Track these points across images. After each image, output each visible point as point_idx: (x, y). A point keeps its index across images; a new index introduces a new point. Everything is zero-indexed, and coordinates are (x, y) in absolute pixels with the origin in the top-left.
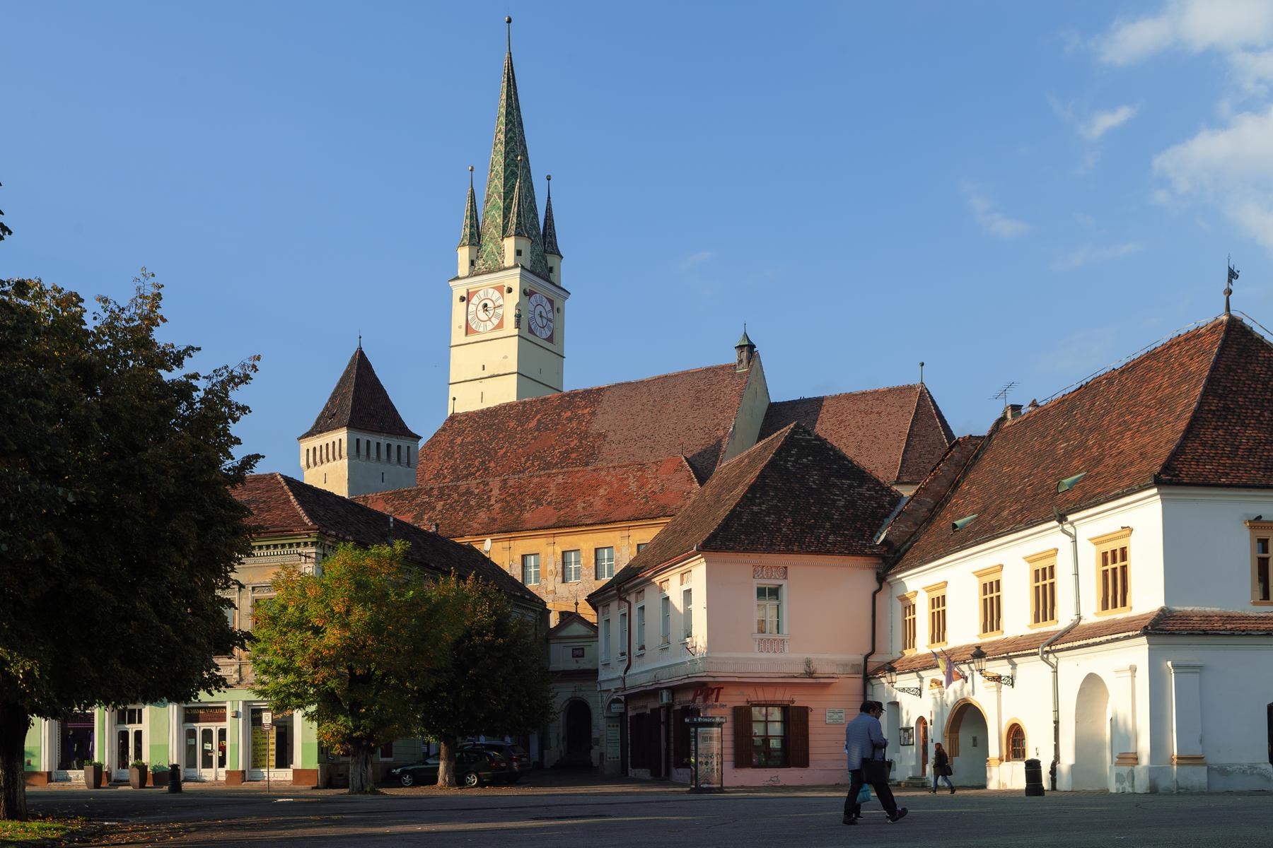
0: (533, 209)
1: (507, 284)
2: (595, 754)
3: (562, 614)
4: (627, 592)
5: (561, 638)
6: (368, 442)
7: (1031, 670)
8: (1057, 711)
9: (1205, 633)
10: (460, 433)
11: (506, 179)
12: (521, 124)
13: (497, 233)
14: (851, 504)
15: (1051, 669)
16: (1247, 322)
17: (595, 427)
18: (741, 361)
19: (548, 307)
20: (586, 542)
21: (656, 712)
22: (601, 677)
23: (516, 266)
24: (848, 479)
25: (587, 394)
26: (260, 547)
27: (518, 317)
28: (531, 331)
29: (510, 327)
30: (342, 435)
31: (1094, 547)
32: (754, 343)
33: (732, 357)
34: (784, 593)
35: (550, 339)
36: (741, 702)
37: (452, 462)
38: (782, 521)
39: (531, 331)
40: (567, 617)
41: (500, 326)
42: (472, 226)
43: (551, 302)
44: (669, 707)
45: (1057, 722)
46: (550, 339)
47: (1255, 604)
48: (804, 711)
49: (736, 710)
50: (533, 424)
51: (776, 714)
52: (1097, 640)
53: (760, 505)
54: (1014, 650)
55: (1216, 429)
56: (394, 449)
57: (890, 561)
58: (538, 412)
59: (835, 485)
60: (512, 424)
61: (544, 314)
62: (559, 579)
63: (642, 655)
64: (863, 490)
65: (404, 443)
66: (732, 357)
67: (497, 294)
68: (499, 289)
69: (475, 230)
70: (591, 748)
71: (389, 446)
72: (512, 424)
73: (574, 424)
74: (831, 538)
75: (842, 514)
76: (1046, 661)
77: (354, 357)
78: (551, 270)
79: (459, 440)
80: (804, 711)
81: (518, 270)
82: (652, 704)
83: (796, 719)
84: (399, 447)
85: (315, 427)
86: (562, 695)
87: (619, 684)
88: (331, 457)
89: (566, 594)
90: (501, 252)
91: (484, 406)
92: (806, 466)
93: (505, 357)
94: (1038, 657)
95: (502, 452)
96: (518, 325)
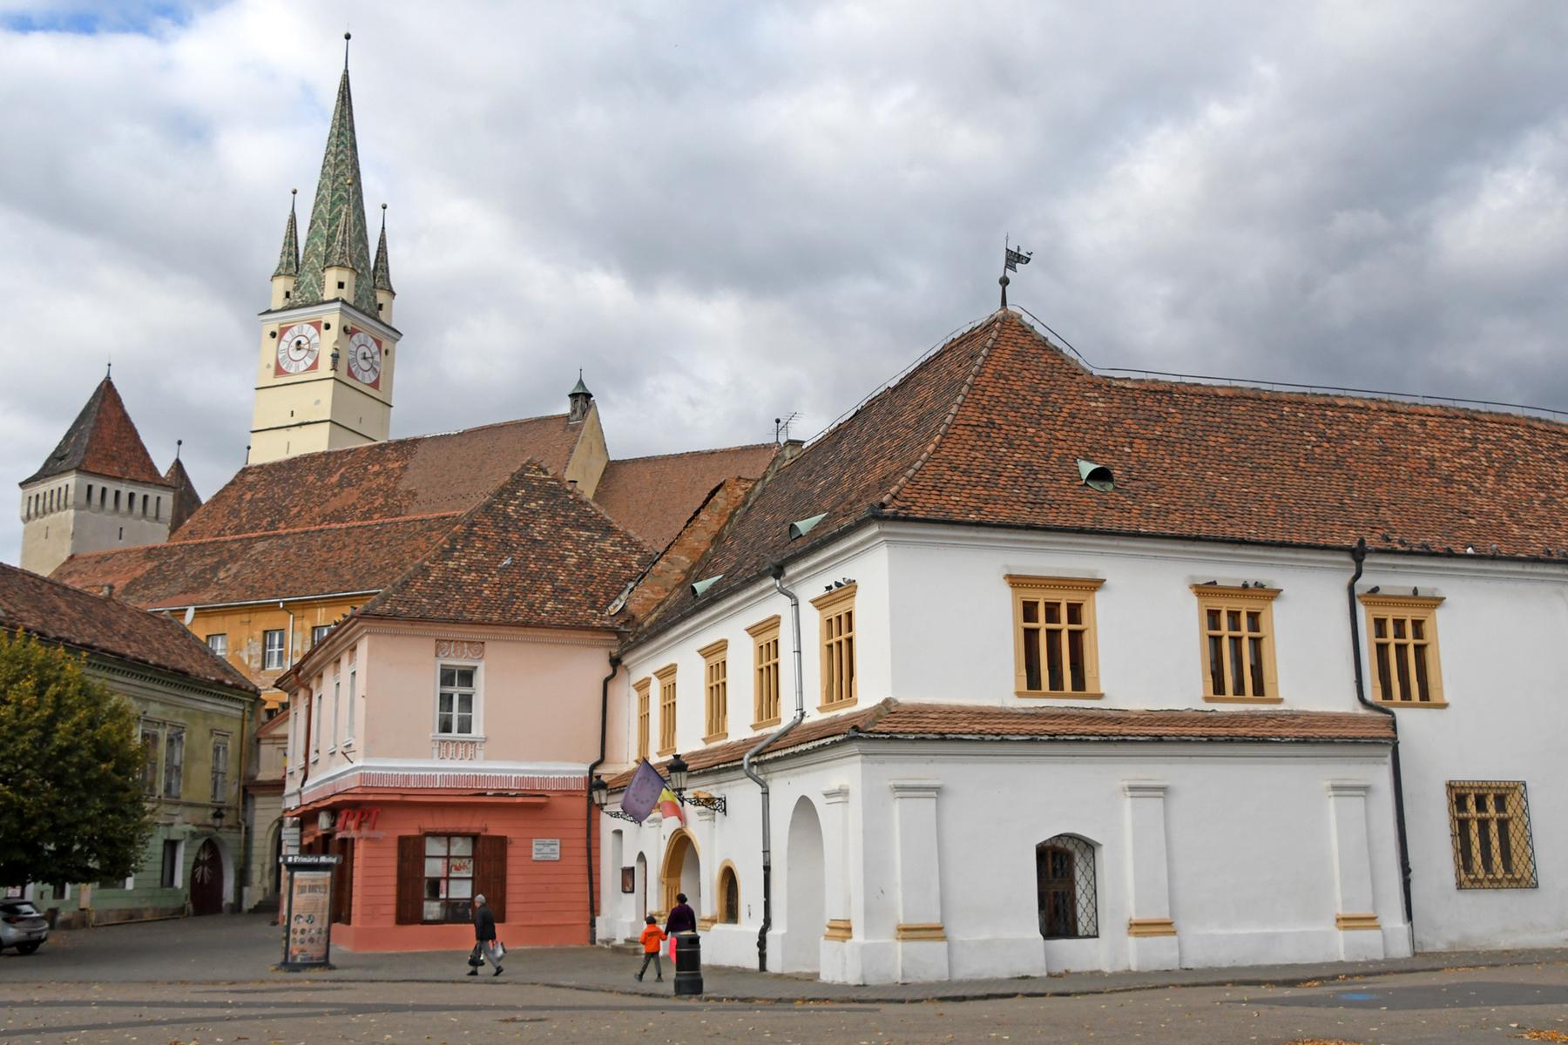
0: (362, 238)
1: (325, 320)
5: (275, 738)
7: (741, 794)
8: (766, 852)
9: (942, 738)
10: (251, 487)
11: (333, 204)
12: (354, 147)
14: (587, 562)
15: (759, 789)
16: (1027, 319)
17: (403, 486)
18: (574, 412)
19: (374, 348)
23: (336, 300)
24: (588, 529)
25: (402, 443)
27: (335, 357)
28: (350, 374)
29: (325, 368)
30: (71, 480)
31: (817, 613)
32: (590, 390)
33: (565, 408)
34: (479, 679)
35: (375, 385)
36: (412, 831)
37: (236, 521)
38: (485, 580)
39: (350, 374)
41: (314, 366)
42: (290, 254)
43: (379, 343)
45: (767, 869)
46: (375, 385)
47: (1019, 694)
48: (502, 842)
49: (402, 841)
50: (335, 479)
51: (461, 847)
52: (803, 747)
54: (725, 763)
55: (973, 448)
56: (138, 500)
57: (628, 638)
58: (341, 466)
59: (568, 537)
60: (311, 478)
64: (607, 545)
66: (565, 408)
67: (313, 330)
68: (316, 325)
69: (292, 259)
71: (131, 496)
72: (311, 478)
73: (381, 480)
74: (549, 605)
75: (571, 574)
76: (755, 779)
77: (99, 389)
78: (380, 307)
79: (248, 496)
80: (502, 842)
81: (338, 305)
83: (491, 859)
84: (117, 493)
85: (42, 469)
90: (321, 284)
91: (289, 456)
92: (532, 512)
93: (318, 402)
94: (741, 774)
95: (295, 510)
96: (334, 368)
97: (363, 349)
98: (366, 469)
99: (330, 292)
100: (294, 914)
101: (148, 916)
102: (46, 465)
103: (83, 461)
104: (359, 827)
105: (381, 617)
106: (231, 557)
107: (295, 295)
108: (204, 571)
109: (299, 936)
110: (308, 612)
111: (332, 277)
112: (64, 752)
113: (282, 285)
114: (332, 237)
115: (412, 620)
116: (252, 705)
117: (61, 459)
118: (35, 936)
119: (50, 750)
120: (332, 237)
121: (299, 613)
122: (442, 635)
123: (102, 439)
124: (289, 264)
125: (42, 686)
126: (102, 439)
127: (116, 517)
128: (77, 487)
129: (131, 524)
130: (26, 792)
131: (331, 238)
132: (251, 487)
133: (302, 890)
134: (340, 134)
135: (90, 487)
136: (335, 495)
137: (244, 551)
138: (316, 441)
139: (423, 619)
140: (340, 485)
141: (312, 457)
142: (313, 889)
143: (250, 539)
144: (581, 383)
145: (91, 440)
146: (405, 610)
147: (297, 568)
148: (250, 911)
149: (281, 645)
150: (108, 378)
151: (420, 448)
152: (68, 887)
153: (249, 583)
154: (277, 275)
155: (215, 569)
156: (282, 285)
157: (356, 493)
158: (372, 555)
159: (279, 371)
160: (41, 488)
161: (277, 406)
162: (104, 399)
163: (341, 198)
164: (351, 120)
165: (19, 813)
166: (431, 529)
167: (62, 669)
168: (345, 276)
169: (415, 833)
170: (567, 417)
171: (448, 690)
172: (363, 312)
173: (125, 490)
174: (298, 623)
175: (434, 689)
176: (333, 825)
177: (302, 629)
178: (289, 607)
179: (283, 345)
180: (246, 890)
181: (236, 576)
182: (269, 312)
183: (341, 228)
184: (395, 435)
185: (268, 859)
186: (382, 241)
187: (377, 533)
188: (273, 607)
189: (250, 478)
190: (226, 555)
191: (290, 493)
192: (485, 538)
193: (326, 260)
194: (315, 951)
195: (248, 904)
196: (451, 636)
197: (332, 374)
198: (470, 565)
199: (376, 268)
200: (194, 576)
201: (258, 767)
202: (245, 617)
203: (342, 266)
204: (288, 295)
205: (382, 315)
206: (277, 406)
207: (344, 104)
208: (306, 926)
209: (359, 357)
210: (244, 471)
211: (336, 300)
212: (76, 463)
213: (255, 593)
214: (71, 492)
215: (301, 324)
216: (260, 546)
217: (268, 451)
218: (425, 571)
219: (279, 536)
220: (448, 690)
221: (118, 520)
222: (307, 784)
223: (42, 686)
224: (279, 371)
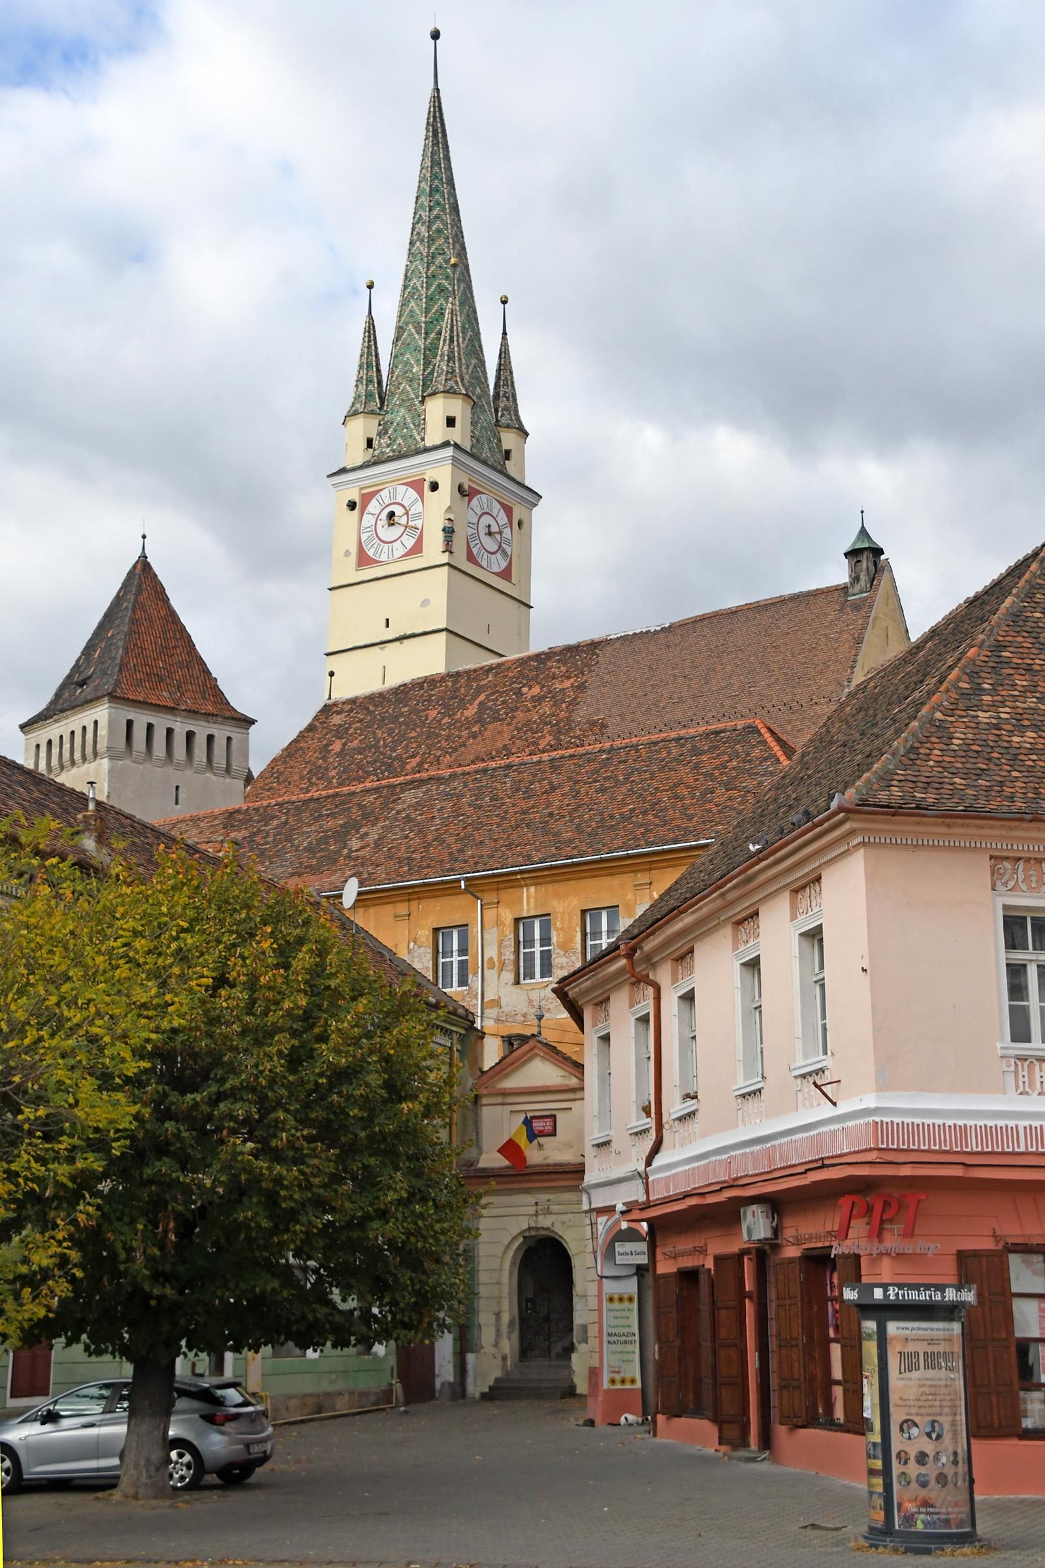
0: (475, 350)
1: (430, 475)
2: (579, 1363)
3: (510, 1041)
4: (651, 961)
5: (505, 1093)
6: (150, 727)
11: (430, 299)
12: (455, 209)
13: (411, 391)
17: (582, 714)
18: (855, 579)
19: (502, 518)
20: (565, 904)
21: (730, 1263)
22: (591, 1177)
23: (446, 444)
25: (571, 651)
26: (940, 1379)
27: (449, 532)
28: (471, 558)
29: (434, 550)
30: (101, 713)
32: (879, 540)
33: (838, 573)
35: (506, 574)
39: (471, 558)
40: (518, 1045)
41: (417, 549)
42: (369, 381)
43: (508, 510)
44: (763, 1254)
46: (506, 574)
50: (471, 711)
53: (994, 705)
56: (200, 742)
60: (432, 714)
61: (494, 529)
62: (509, 976)
63: (691, 1115)
65: (221, 733)
66: (838, 573)
67: (412, 494)
68: (417, 485)
69: (373, 388)
70: (571, 1349)
71: (190, 736)
72: (432, 714)
73: (546, 708)
77: (131, 574)
78: (507, 455)
79: (337, 746)
81: (449, 452)
82: (719, 1245)
85: (47, 709)
86: (499, 1229)
87: (636, 1193)
88: (77, 755)
89: (523, 1007)
90: (420, 423)
93: (425, 603)
96: (448, 549)
97: (486, 520)
98: (519, 693)
99: (436, 432)
100: (896, 1417)
101: (342, 1406)
102: (58, 695)
103: (117, 683)
104: (878, 1233)
105: (891, 810)
106: (365, 816)
107: (381, 443)
108: (324, 840)
109: (913, 1469)
110: (505, 895)
111: (436, 409)
112: (341, 1076)
113: (363, 427)
114: (431, 350)
115: (949, 816)
116: (462, 1039)
117: (81, 684)
118: (256, 1449)
119: (313, 1073)
120: (431, 350)
121: (491, 897)
122: (1002, 847)
123: (141, 651)
124: (369, 396)
125: (285, 953)
126: (141, 651)
127: (170, 770)
128: (111, 723)
129: (190, 779)
130: (276, 1156)
131: (431, 351)
132: (341, 732)
133: (910, 1362)
134: (433, 190)
135: (130, 724)
136: (474, 736)
137: (385, 806)
138: (428, 660)
139: (971, 814)
140: (479, 719)
141: (431, 682)
142: (931, 1360)
143: (392, 787)
144: (863, 533)
145: (126, 650)
146: (931, 798)
147: (478, 826)
148: (484, 1396)
149: (463, 951)
150: (144, 556)
151: (604, 656)
152: (229, 1356)
153: (402, 853)
154: (353, 414)
155: (342, 836)
156: (363, 427)
157: (507, 731)
158: (603, 798)
159: (364, 560)
160: (54, 731)
161: (363, 612)
162: (140, 590)
163: (441, 289)
164: (449, 168)
165: (272, 1200)
166: (696, 751)
167: (307, 923)
168: (457, 407)
169: (988, 1244)
170: (844, 589)
171: (1018, 956)
172: (484, 462)
173: (181, 727)
174: (490, 914)
175: (997, 956)
176: (776, 1231)
177: (498, 922)
178: (474, 888)
179: (368, 520)
180: (470, 1358)
181: (378, 845)
182: (343, 471)
183: (445, 334)
184: (537, 645)
185: (505, 1305)
186: (504, 353)
187: (605, 764)
188: (451, 888)
189: (337, 720)
190: (356, 813)
191: (403, 737)
192: (1029, 669)
193: (425, 386)
194: (949, 1504)
195: (476, 1387)
196: (1019, 848)
197: (445, 558)
198: (1018, 716)
199: (497, 396)
200: (308, 849)
201: (479, 1147)
202: (402, 909)
203: (450, 392)
204: (370, 443)
205: (510, 466)
206: (363, 612)
207: (436, 144)
208: (929, 1447)
209: (482, 531)
210: (327, 710)
211: (446, 444)
212: (108, 687)
213: (415, 869)
214: (103, 732)
215: (393, 485)
216: (410, 797)
217: (360, 678)
218: (943, 732)
219: (439, 780)
220: (1018, 956)
221: (175, 776)
222: (658, 1161)
223: (285, 953)
224: (364, 560)
